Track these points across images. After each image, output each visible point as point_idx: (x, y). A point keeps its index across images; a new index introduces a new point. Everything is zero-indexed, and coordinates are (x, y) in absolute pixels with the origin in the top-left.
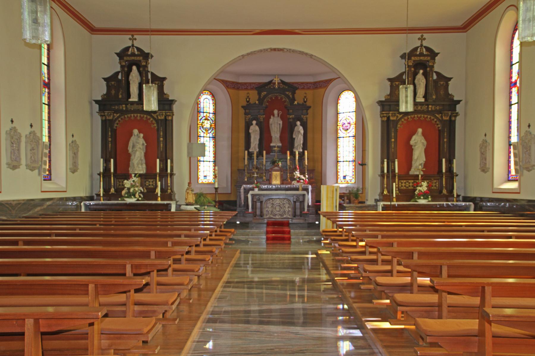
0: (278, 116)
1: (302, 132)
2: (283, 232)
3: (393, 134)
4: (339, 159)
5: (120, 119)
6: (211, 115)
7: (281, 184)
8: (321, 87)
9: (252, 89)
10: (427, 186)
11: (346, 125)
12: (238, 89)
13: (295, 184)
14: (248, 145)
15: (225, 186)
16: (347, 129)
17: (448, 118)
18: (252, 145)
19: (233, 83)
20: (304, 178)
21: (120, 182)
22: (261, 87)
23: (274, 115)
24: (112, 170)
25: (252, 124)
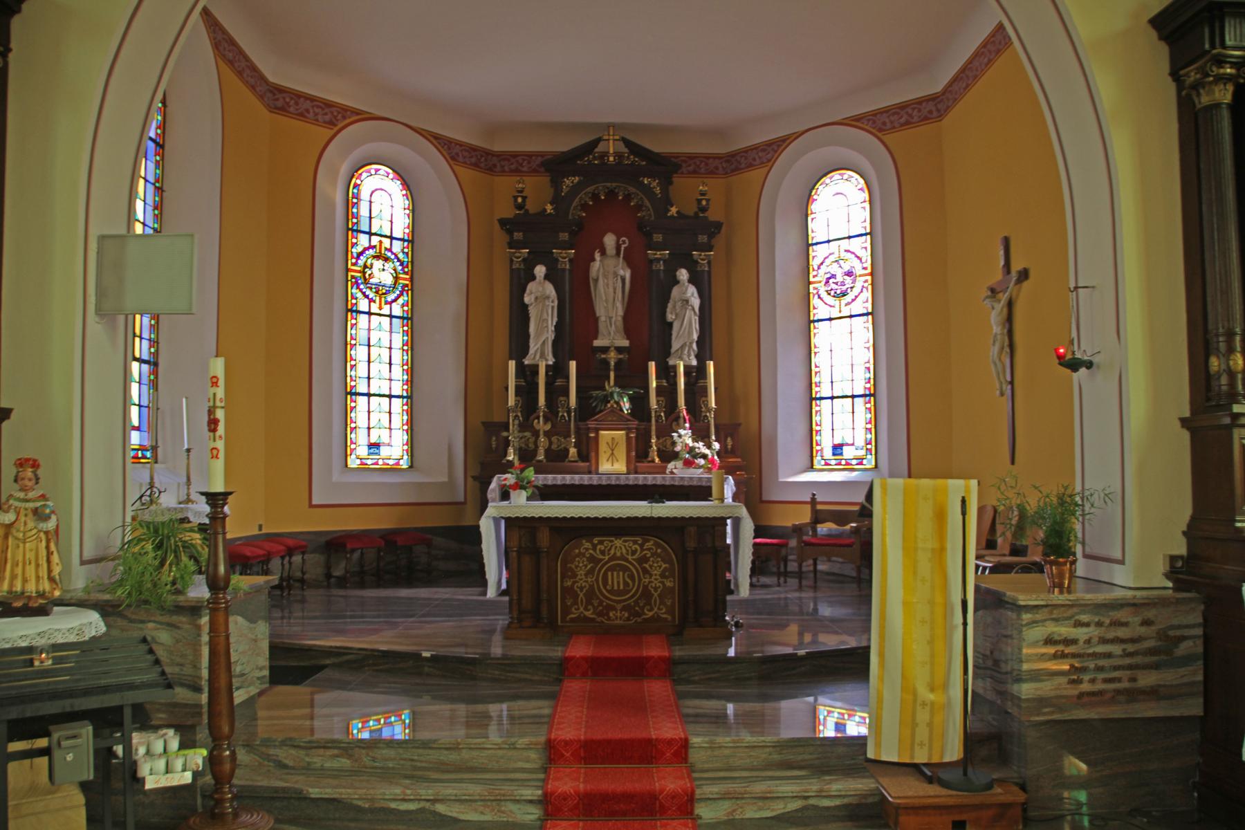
0: (618, 254)
1: (696, 302)
2: (646, 752)
4: (815, 389)
6: (397, 247)
8: (750, 166)
9: (534, 171)
11: (839, 279)
12: (491, 170)
13: (676, 469)
14: (519, 345)
15: (446, 480)
16: (844, 294)
18: (534, 347)
19: (473, 149)
20: (707, 452)
22: (556, 166)
23: (603, 253)
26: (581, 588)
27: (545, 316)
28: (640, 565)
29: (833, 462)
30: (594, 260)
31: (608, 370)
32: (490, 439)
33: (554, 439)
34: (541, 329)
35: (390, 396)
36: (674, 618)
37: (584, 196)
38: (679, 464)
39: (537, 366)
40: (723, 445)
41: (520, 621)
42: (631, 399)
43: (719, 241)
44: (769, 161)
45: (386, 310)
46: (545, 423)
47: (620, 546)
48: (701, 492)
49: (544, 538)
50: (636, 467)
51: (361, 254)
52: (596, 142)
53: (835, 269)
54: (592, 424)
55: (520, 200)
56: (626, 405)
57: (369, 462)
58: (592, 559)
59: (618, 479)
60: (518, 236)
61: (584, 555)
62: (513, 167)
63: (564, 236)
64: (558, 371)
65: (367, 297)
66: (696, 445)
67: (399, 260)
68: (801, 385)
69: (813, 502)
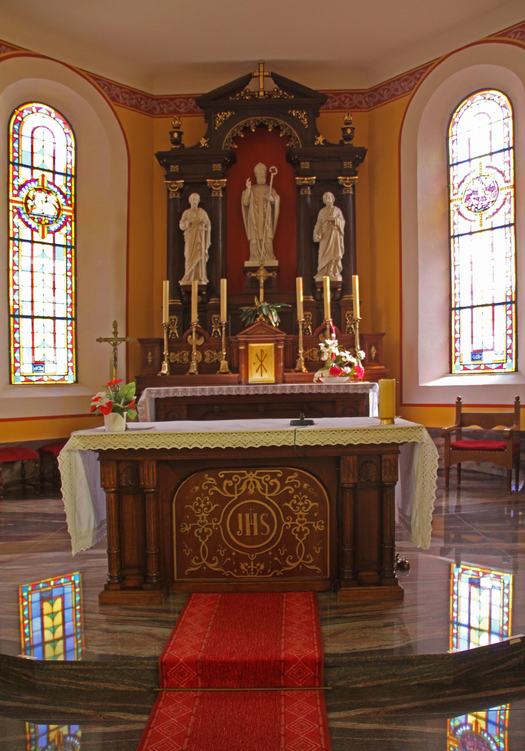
0: (268, 182)
1: (341, 223)
7: (277, 383)
9: (191, 112)
11: (481, 194)
12: (150, 112)
14: (176, 267)
16: (485, 208)
18: (188, 268)
19: (133, 92)
20: (353, 360)
22: (207, 104)
23: (254, 182)
25: (188, 206)
26: (203, 535)
27: (199, 239)
28: (280, 504)
29: (472, 367)
30: (245, 188)
31: (258, 288)
32: (146, 354)
33: (207, 353)
34: (195, 252)
35: (54, 318)
36: (324, 572)
37: (236, 130)
38: (326, 372)
39: (190, 286)
40: (369, 354)
41: (122, 578)
42: (280, 314)
43: (363, 168)
44: (411, 89)
45: (49, 238)
46: (198, 338)
47: (253, 480)
48: (356, 405)
49: (149, 476)
50: (284, 377)
51: (23, 186)
53: (477, 186)
54: (241, 337)
55: (176, 135)
56: (274, 319)
57: (34, 379)
58: (217, 498)
59: (265, 389)
60: (174, 168)
61: (206, 493)
62: (171, 109)
63: (217, 167)
64: (210, 291)
65: (30, 226)
66: (342, 354)
67: (62, 193)
68: (442, 297)
69: (459, 405)
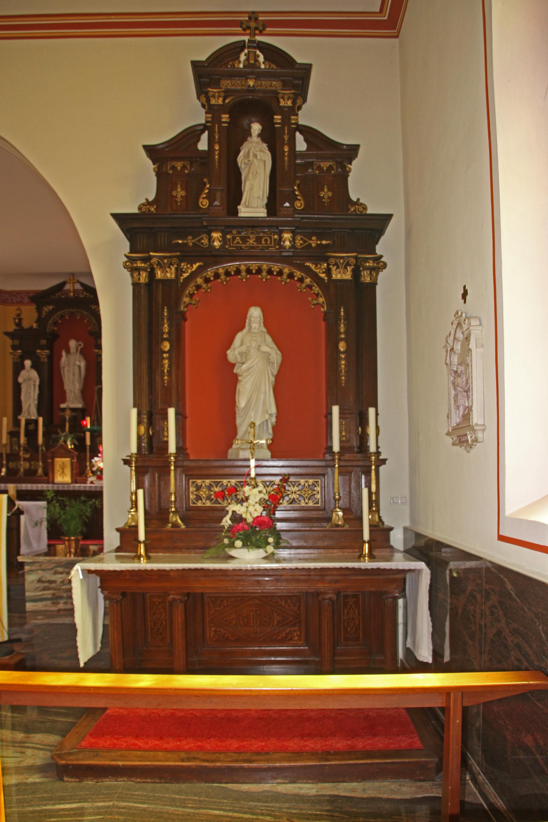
0: (77, 350)
3: (166, 328)
5: (308, 281)
10: (260, 502)
17: (348, 276)
21: (198, 488)
22: (39, 299)
23: (68, 351)
24: (172, 448)
52: (64, 284)
55: (17, 321)
59: (58, 487)
62: (19, 300)
63: (44, 342)
